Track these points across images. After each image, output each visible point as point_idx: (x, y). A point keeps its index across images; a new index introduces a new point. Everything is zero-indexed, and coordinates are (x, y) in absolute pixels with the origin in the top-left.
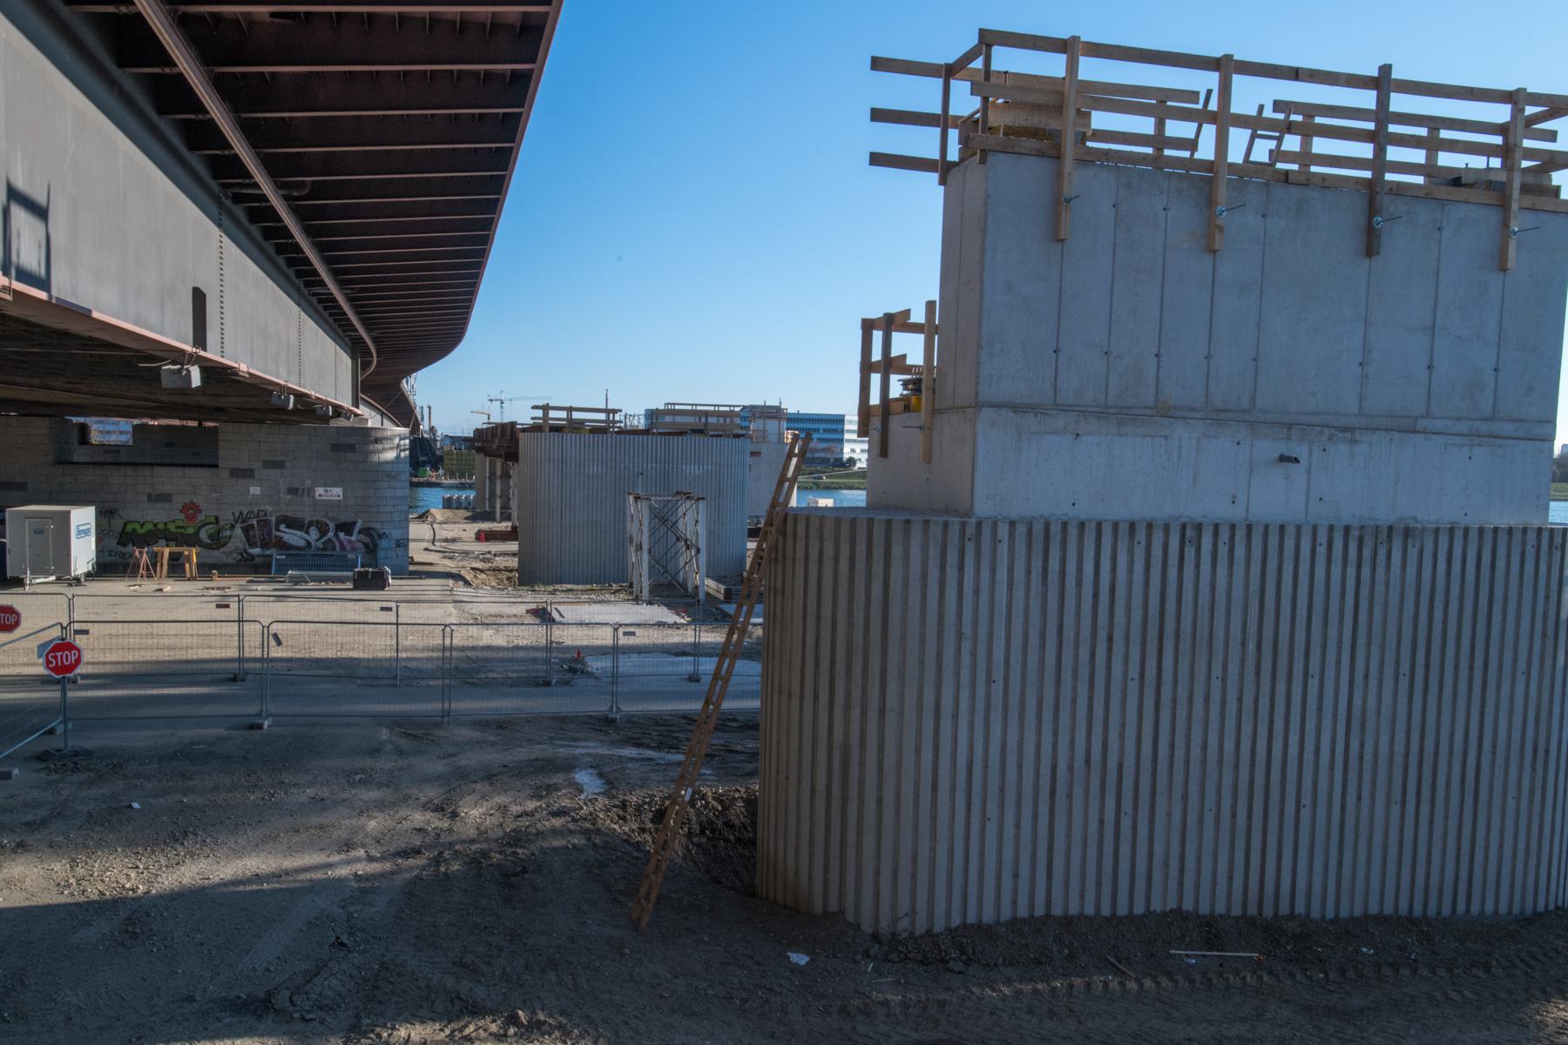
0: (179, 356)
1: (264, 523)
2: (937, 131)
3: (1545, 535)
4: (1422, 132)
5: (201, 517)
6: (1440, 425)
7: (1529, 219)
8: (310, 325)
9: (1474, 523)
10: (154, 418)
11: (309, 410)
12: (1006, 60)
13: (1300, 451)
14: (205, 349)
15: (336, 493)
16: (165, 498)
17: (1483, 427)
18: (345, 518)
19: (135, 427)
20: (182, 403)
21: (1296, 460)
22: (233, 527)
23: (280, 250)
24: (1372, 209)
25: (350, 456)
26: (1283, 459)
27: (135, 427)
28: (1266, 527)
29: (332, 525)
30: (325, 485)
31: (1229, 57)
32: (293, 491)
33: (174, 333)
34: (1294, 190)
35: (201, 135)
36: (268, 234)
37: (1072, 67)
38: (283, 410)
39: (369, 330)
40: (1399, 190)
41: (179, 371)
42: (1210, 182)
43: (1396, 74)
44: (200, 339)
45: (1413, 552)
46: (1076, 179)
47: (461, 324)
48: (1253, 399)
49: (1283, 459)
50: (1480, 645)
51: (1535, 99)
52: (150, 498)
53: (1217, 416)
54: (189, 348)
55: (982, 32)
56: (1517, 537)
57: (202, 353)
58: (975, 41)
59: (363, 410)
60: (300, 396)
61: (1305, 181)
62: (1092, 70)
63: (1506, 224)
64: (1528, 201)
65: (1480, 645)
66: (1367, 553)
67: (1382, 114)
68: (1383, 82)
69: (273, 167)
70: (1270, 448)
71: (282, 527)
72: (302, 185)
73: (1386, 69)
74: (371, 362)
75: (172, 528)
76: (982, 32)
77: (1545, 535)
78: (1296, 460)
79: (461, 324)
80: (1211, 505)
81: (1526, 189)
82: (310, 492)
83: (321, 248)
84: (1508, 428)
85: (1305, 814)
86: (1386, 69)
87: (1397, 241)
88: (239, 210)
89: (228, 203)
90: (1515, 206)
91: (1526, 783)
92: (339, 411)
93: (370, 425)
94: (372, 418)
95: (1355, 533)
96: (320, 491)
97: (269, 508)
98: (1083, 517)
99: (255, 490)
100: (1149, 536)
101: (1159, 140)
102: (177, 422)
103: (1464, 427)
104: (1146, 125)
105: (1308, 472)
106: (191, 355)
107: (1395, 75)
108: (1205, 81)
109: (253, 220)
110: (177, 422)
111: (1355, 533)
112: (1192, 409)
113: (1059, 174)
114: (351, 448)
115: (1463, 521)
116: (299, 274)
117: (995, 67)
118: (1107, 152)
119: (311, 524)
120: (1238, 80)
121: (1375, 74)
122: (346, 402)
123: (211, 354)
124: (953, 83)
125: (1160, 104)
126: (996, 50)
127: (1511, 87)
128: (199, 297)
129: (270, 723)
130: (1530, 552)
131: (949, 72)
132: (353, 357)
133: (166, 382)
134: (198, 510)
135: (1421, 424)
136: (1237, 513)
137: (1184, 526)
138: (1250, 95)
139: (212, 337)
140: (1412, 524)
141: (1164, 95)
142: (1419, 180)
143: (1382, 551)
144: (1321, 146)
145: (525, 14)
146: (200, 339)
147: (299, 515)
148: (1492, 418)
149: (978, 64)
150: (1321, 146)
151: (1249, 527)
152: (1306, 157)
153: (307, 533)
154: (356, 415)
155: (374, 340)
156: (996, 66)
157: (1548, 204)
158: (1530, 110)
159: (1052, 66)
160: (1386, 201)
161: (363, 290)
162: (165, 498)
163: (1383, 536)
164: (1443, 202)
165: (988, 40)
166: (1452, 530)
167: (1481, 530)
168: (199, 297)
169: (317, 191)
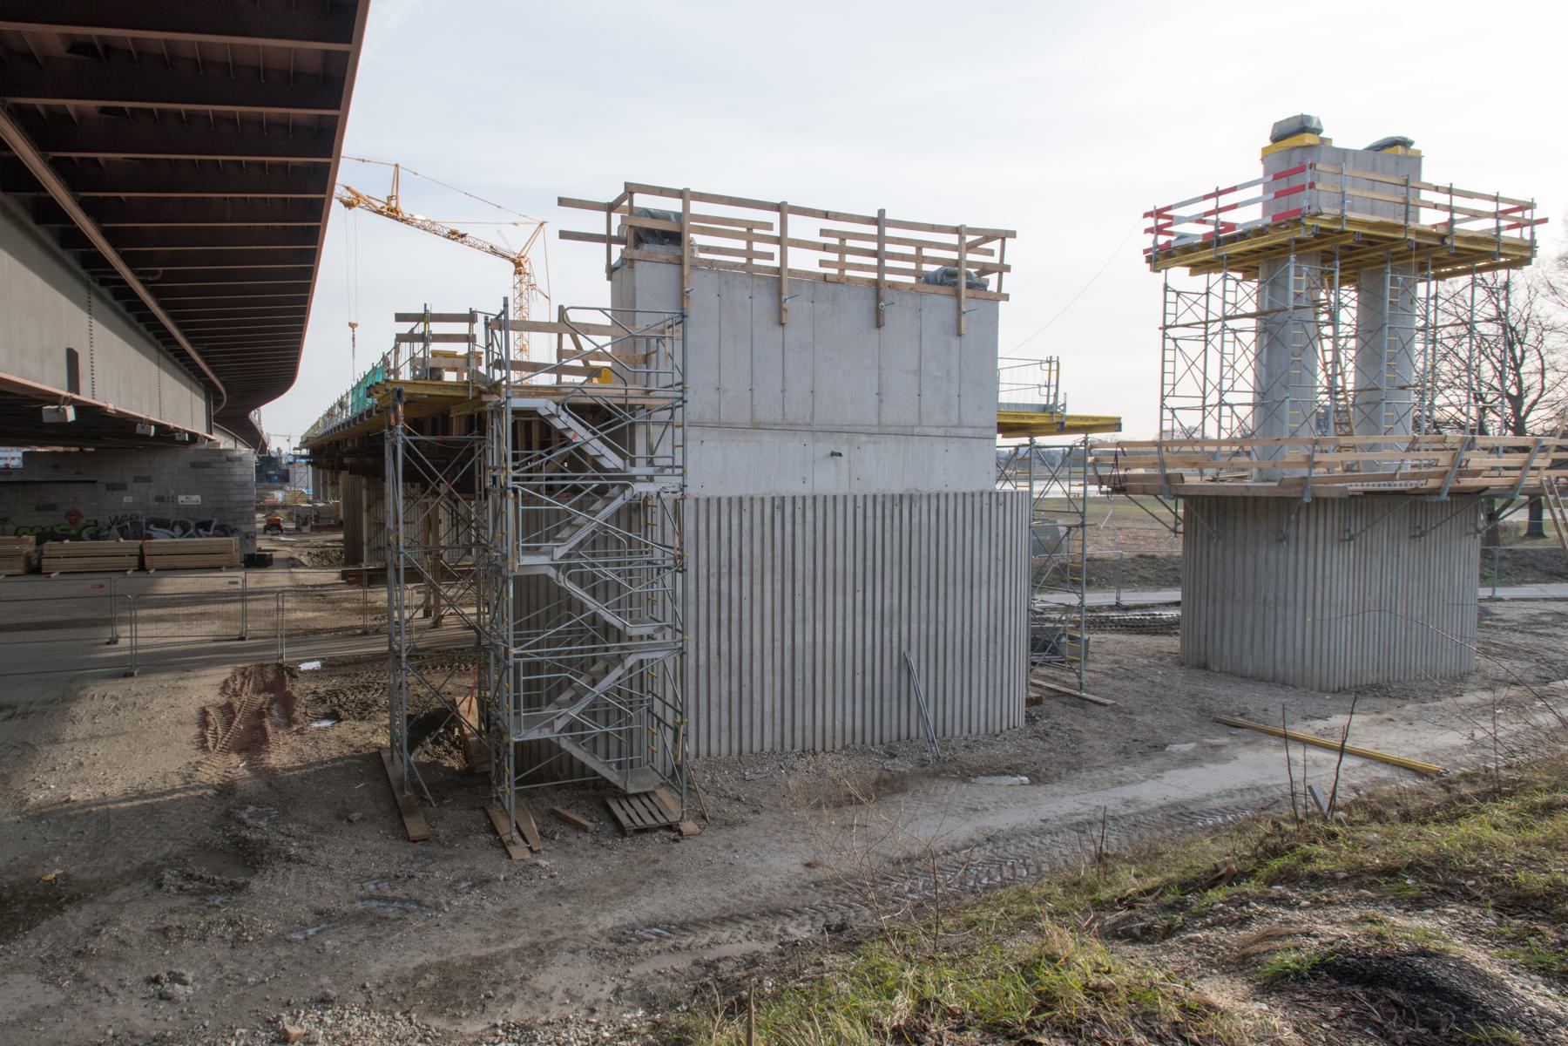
0: (54, 399)
1: (136, 524)
2: (604, 246)
3: (994, 496)
4: (911, 250)
5: (83, 521)
6: (929, 431)
7: (973, 304)
8: (168, 379)
9: (951, 489)
10: (41, 446)
11: (166, 437)
12: (641, 201)
13: (844, 450)
14: (78, 393)
15: (196, 499)
16: (52, 507)
17: (954, 432)
18: (203, 518)
19: (24, 453)
20: (61, 432)
21: (840, 455)
22: (109, 528)
23: (140, 319)
24: (878, 299)
25: (207, 471)
26: (833, 454)
27: (24, 453)
28: (825, 497)
29: (192, 524)
30: (186, 493)
31: (784, 203)
32: (160, 499)
33: (51, 380)
34: (831, 287)
35: (71, 238)
36: (130, 307)
37: (686, 207)
38: (146, 437)
39: (218, 376)
40: (893, 286)
41: (57, 410)
42: (780, 281)
43: (887, 216)
44: (74, 384)
45: (915, 510)
46: (695, 282)
47: (295, 337)
48: (812, 418)
49: (833, 454)
50: (942, 558)
51: (973, 231)
52: (38, 508)
53: (788, 427)
54: (64, 393)
55: (627, 185)
56: (977, 498)
57: (76, 397)
58: (621, 190)
59: (215, 437)
60: (159, 427)
61: (840, 281)
62: (697, 208)
63: (959, 307)
64: (971, 292)
65: (942, 558)
66: (887, 512)
67: (881, 239)
68: (879, 221)
69: (129, 259)
70: (825, 447)
71: (152, 527)
72: (156, 272)
73: (882, 212)
74: (222, 401)
75: (57, 530)
76: (627, 185)
77: (994, 496)
78: (840, 455)
79: (295, 337)
80: (791, 486)
81: (969, 286)
82: (174, 499)
83: (173, 317)
84: (968, 432)
85: (858, 678)
86: (882, 212)
87: (892, 316)
88: (105, 291)
89: (96, 286)
90: (963, 297)
91: (991, 651)
92: (194, 437)
93: (222, 447)
94: (224, 442)
95: (879, 500)
96: (181, 498)
97: (140, 513)
98: (709, 495)
99: (128, 499)
100: (752, 506)
101: (750, 254)
102: (61, 449)
103: (941, 432)
104: (741, 245)
105: (849, 462)
106: (66, 398)
107: (887, 216)
108: (773, 217)
109: (117, 298)
110: (61, 449)
111: (879, 500)
112: (775, 424)
113: (682, 276)
114: (207, 465)
115: (945, 490)
116: (164, 344)
117: (635, 205)
118: (712, 262)
119: (175, 524)
120: (791, 218)
121: (876, 216)
122: (201, 429)
123: (84, 396)
124: (613, 214)
125: (749, 231)
126: (636, 196)
127: (957, 224)
128: (72, 357)
129: (238, 470)
130: (986, 508)
131: (610, 208)
132: (207, 400)
133: (47, 418)
134: (79, 515)
135: (916, 430)
136: (807, 490)
137: (773, 498)
138: (800, 228)
139: (84, 384)
140: (914, 492)
141: (751, 225)
142: (911, 280)
143: (897, 510)
144: (849, 258)
145: (327, 53)
146: (74, 384)
147: (166, 517)
148: (959, 426)
149: (626, 203)
150: (849, 258)
151: (814, 498)
152: (842, 266)
153: (172, 530)
154: (210, 440)
155: (223, 383)
156: (636, 204)
157: (982, 294)
158: (969, 238)
159: (674, 205)
160: (885, 292)
161: (210, 347)
162: (52, 507)
163: (897, 501)
164: (921, 294)
165: (630, 190)
166: (938, 496)
167: (956, 495)
168: (72, 357)
169: (167, 277)
